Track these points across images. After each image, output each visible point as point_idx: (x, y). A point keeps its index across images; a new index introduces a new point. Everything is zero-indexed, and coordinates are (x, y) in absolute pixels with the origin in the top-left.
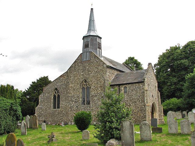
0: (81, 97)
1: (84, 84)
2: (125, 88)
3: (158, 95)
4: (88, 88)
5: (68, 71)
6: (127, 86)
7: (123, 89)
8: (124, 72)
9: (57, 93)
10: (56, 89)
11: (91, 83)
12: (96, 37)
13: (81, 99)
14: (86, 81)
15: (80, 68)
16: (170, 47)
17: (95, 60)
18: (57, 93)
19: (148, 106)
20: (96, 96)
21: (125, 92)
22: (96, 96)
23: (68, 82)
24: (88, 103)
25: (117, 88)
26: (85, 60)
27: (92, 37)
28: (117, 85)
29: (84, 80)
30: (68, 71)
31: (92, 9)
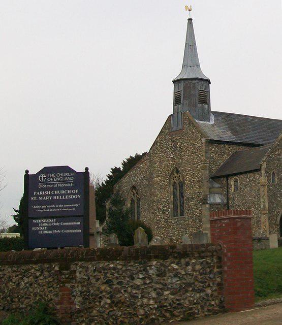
0: (171, 202)
1: (175, 177)
2: (236, 181)
3: (139, 207)
4: (182, 185)
5: (151, 152)
6: (239, 178)
7: (232, 183)
8: (259, 145)
9: (136, 194)
10: (134, 187)
11: (185, 174)
12: (193, 82)
13: (171, 206)
14: (177, 172)
15: (169, 144)
16: (87, 169)
17: (190, 130)
18: (136, 194)
19: (264, 214)
20: (193, 198)
21: (236, 188)
22: (193, 198)
23: (152, 174)
24: (182, 214)
25: (224, 181)
26: (175, 128)
27: (186, 82)
28: (223, 176)
29: (175, 170)
30: (151, 152)
31: (190, 20)
